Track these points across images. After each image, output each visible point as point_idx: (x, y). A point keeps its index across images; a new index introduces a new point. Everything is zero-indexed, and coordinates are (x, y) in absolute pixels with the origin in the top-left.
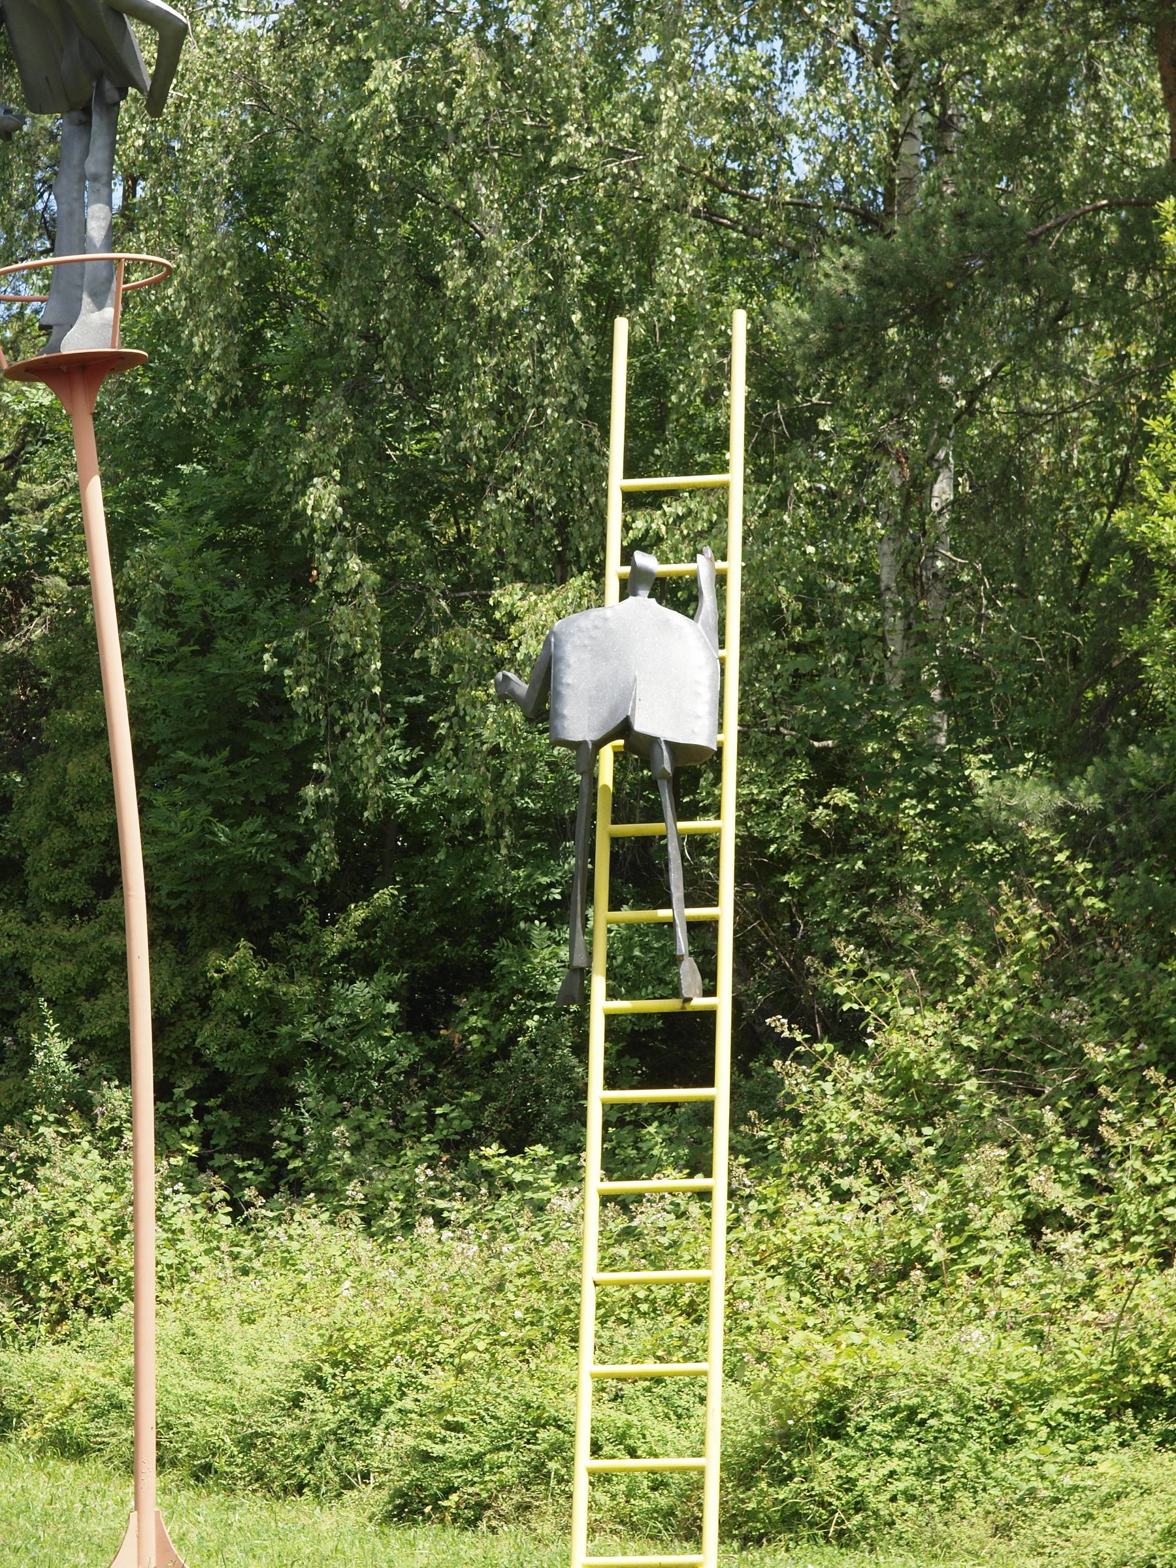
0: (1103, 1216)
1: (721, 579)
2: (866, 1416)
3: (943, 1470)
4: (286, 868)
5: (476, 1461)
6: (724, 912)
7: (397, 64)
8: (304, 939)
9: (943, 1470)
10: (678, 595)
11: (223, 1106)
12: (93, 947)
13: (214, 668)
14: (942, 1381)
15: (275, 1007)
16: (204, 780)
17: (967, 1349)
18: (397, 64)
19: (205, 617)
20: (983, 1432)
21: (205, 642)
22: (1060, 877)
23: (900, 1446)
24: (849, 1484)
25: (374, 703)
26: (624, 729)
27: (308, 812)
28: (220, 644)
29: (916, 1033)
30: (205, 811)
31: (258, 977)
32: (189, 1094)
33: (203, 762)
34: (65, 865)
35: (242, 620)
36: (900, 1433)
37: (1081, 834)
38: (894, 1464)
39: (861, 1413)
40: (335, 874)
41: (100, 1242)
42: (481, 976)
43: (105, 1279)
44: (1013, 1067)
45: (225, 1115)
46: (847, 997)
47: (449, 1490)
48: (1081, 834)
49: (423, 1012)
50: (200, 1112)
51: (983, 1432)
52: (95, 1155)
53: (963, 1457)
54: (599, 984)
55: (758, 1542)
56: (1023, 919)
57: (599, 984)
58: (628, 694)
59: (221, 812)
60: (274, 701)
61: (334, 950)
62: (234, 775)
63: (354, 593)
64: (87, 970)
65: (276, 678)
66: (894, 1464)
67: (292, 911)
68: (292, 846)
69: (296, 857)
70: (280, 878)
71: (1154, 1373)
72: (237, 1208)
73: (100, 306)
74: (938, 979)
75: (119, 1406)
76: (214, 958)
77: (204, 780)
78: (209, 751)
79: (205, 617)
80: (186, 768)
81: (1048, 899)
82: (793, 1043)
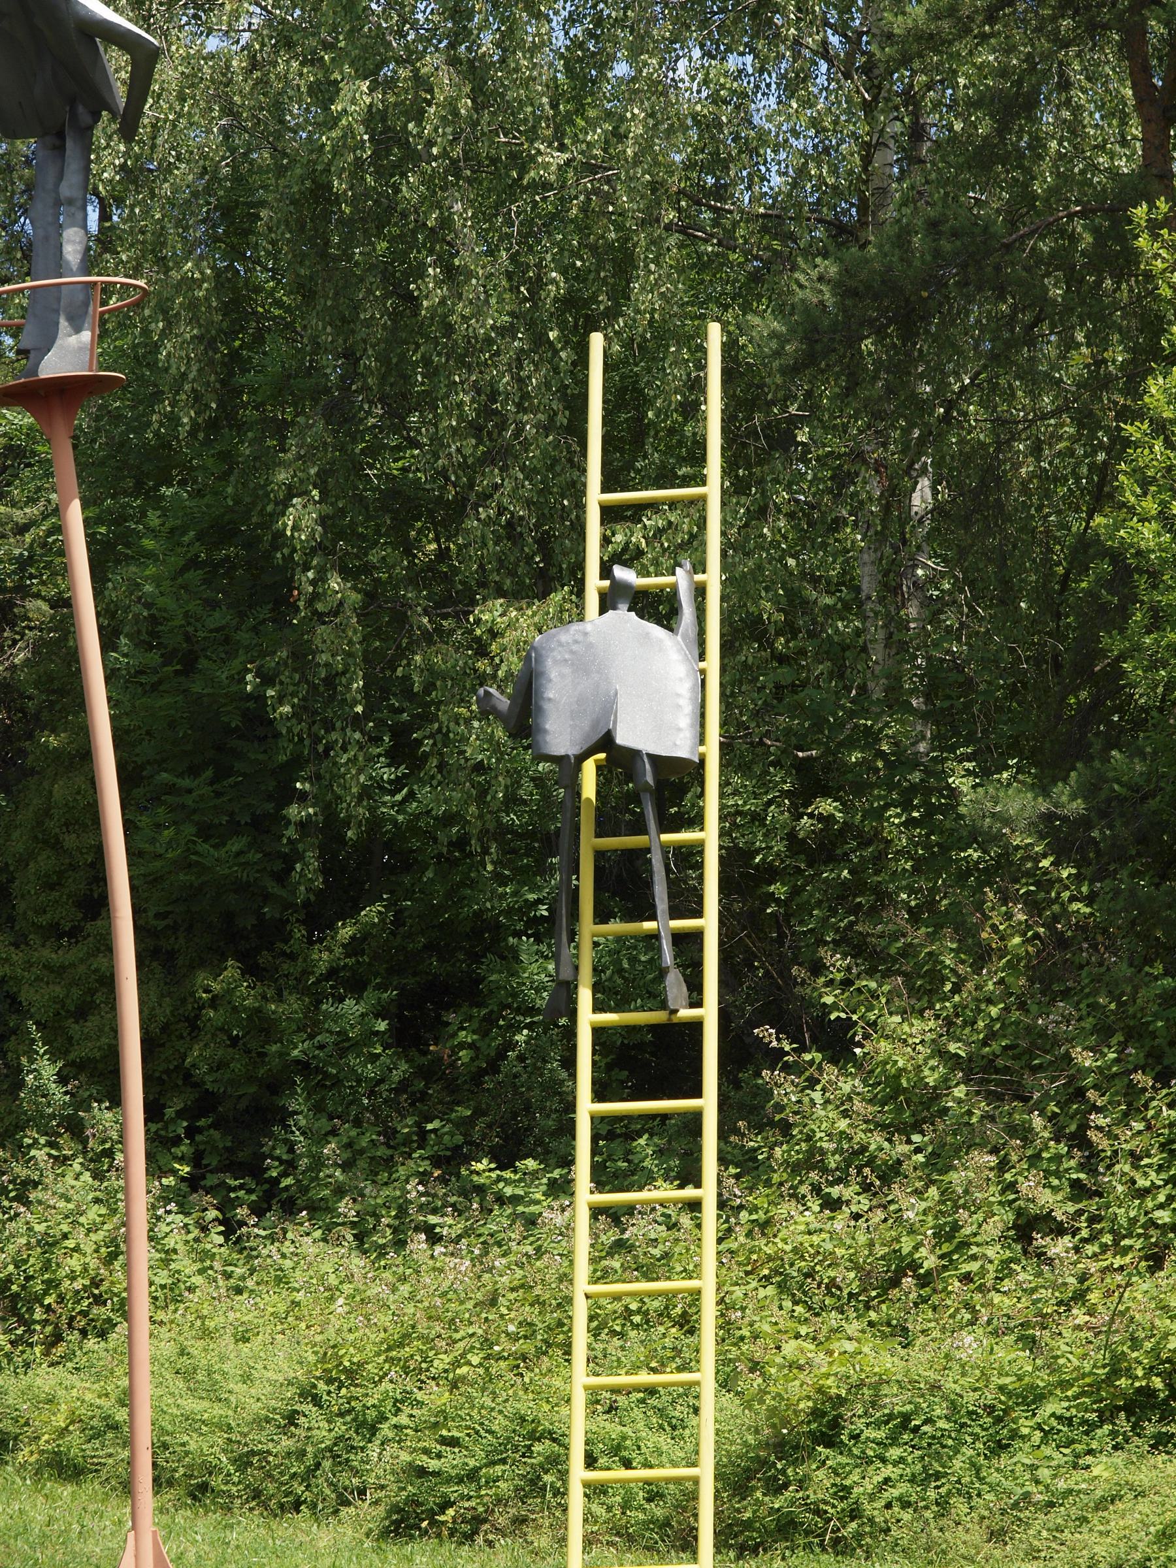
0: (1092, 1220)
1: (700, 592)
2: (860, 1424)
3: (938, 1476)
4: (273, 888)
5: (472, 1475)
6: (709, 923)
7: (365, 86)
8: (292, 957)
9: (938, 1476)
10: (658, 608)
11: (214, 1126)
12: (82, 969)
13: (197, 688)
14: (935, 1387)
15: (263, 1027)
16: (189, 800)
17: (964, 1356)
18: (365, 86)
19: (188, 638)
20: (976, 1437)
21: (189, 665)
22: (1045, 882)
23: (894, 1453)
24: (843, 1492)
25: (357, 722)
26: (606, 742)
27: (291, 832)
28: (203, 663)
29: (904, 1040)
30: (189, 830)
31: (247, 994)
32: (180, 1114)
33: (186, 783)
34: (52, 887)
35: (225, 641)
36: (894, 1440)
37: (1062, 836)
38: (888, 1471)
39: (856, 1421)
40: (319, 893)
41: (93, 1263)
42: (469, 991)
43: (99, 1301)
44: (1002, 1073)
45: (216, 1134)
46: (835, 1007)
47: (446, 1505)
48: (1062, 836)
49: (412, 1029)
50: (191, 1132)
51: (976, 1437)
52: (87, 1177)
53: (957, 1463)
54: (585, 997)
55: (755, 1551)
56: (1009, 926)
57: (585, 997)
58: (609, 708)
59: (205, 832)
60: (256, 717)
61: (323, 968)
62: (218, 794)
63: (337, 611)
64: (76, 992)
65: (258, 697)
66: (888, 1471)
67: (276, 931)
68: (278, 866)
69: (281, 877)
70: (267, 897)
71: (1147, 1376)
72: (230, 1227)
73: (78, 330)
74: (925, 987)
75: (115, 1427)
76: (202, 978)
77: (189, 800)
78: (194, 771)
79: (188, 638)
80: (171, 789)
81: (1033, 906)
82: (782, 1053)
